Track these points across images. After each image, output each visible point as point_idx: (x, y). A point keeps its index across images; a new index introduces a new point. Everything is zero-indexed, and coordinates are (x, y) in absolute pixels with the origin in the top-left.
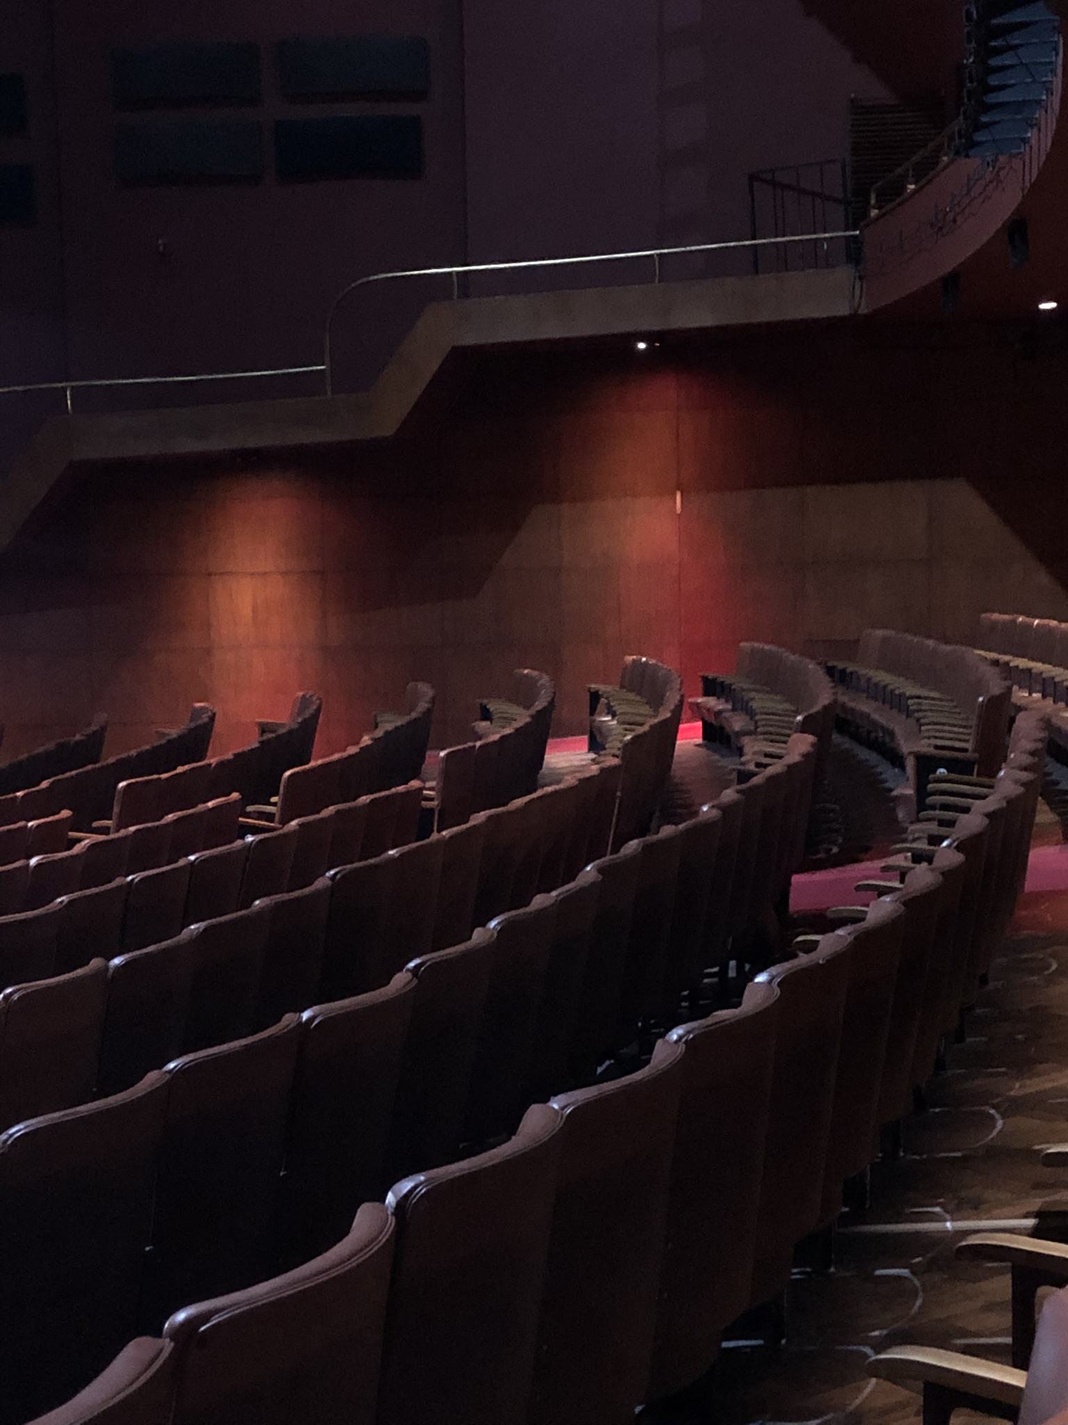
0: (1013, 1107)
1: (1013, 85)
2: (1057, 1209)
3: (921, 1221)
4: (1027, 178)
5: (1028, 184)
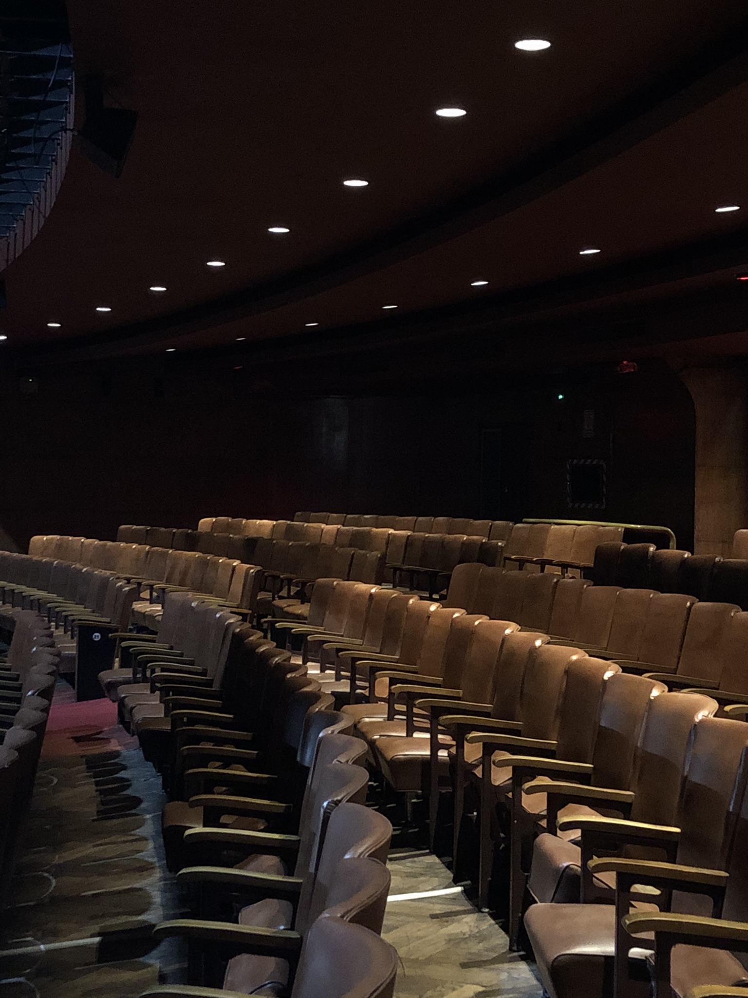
0: (59, 871)
1: (48, 122)
2: (592, 796)
3: (21, 947)
4: (11, 252)
5: (11, 257)
